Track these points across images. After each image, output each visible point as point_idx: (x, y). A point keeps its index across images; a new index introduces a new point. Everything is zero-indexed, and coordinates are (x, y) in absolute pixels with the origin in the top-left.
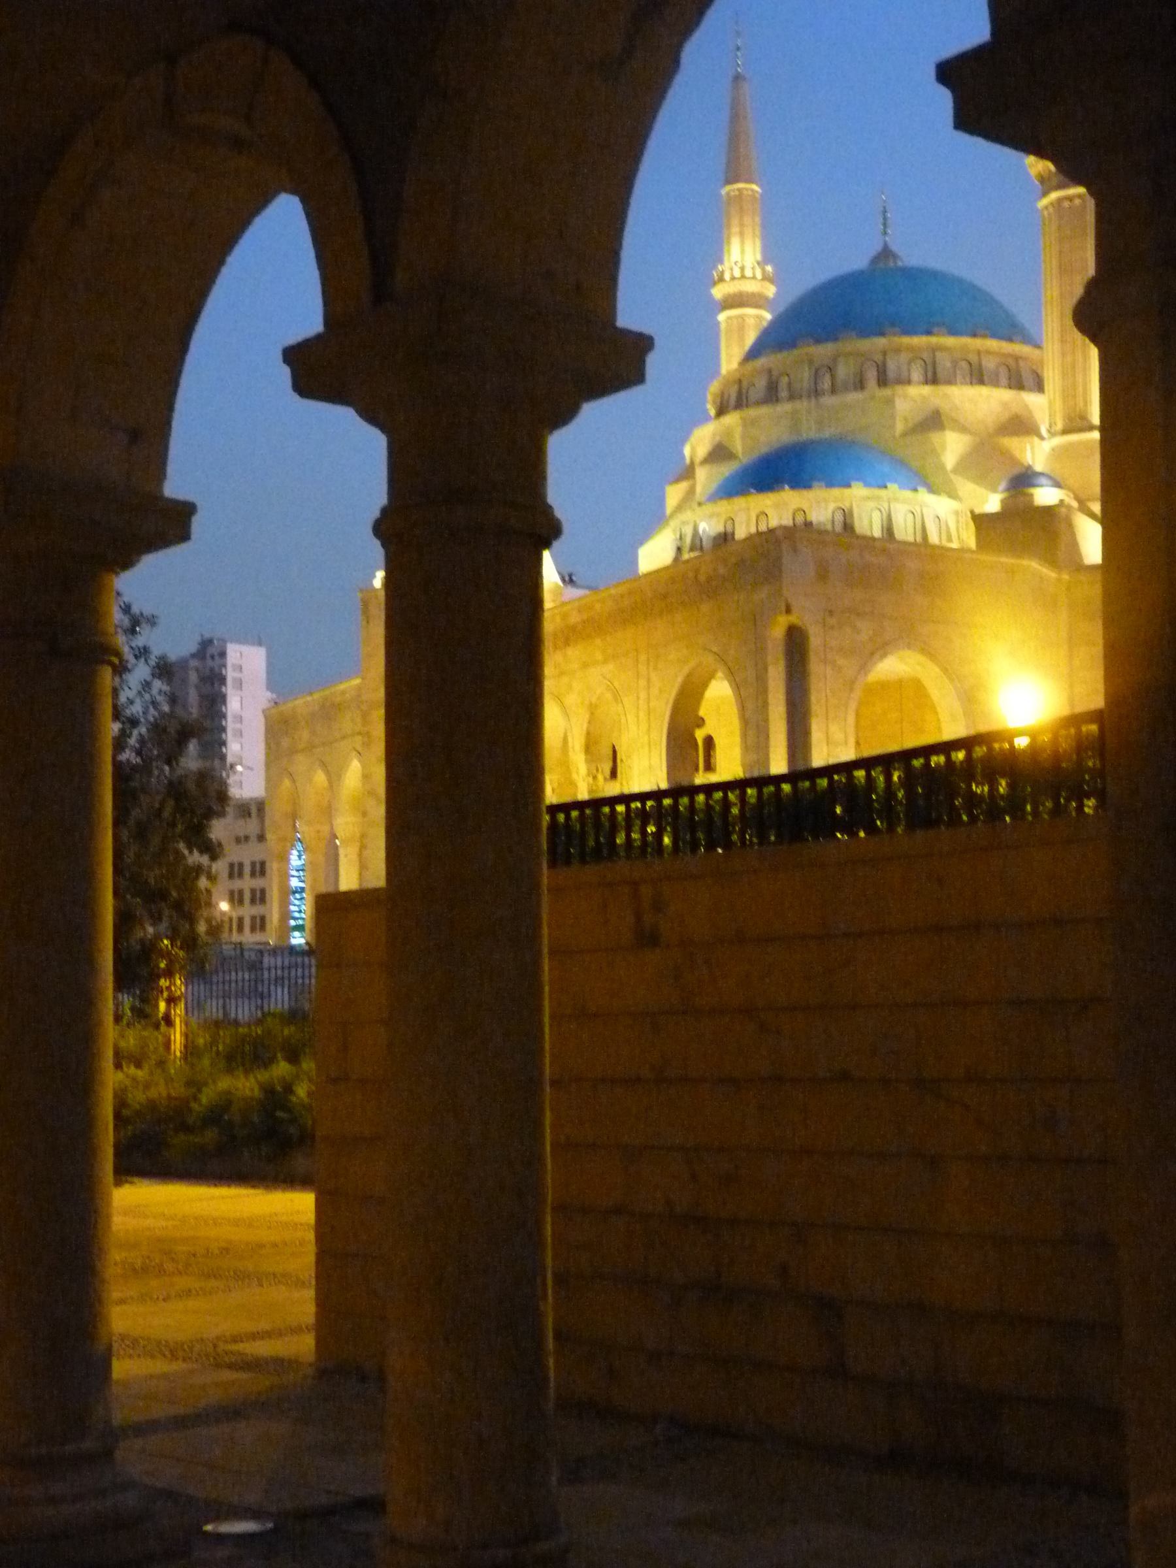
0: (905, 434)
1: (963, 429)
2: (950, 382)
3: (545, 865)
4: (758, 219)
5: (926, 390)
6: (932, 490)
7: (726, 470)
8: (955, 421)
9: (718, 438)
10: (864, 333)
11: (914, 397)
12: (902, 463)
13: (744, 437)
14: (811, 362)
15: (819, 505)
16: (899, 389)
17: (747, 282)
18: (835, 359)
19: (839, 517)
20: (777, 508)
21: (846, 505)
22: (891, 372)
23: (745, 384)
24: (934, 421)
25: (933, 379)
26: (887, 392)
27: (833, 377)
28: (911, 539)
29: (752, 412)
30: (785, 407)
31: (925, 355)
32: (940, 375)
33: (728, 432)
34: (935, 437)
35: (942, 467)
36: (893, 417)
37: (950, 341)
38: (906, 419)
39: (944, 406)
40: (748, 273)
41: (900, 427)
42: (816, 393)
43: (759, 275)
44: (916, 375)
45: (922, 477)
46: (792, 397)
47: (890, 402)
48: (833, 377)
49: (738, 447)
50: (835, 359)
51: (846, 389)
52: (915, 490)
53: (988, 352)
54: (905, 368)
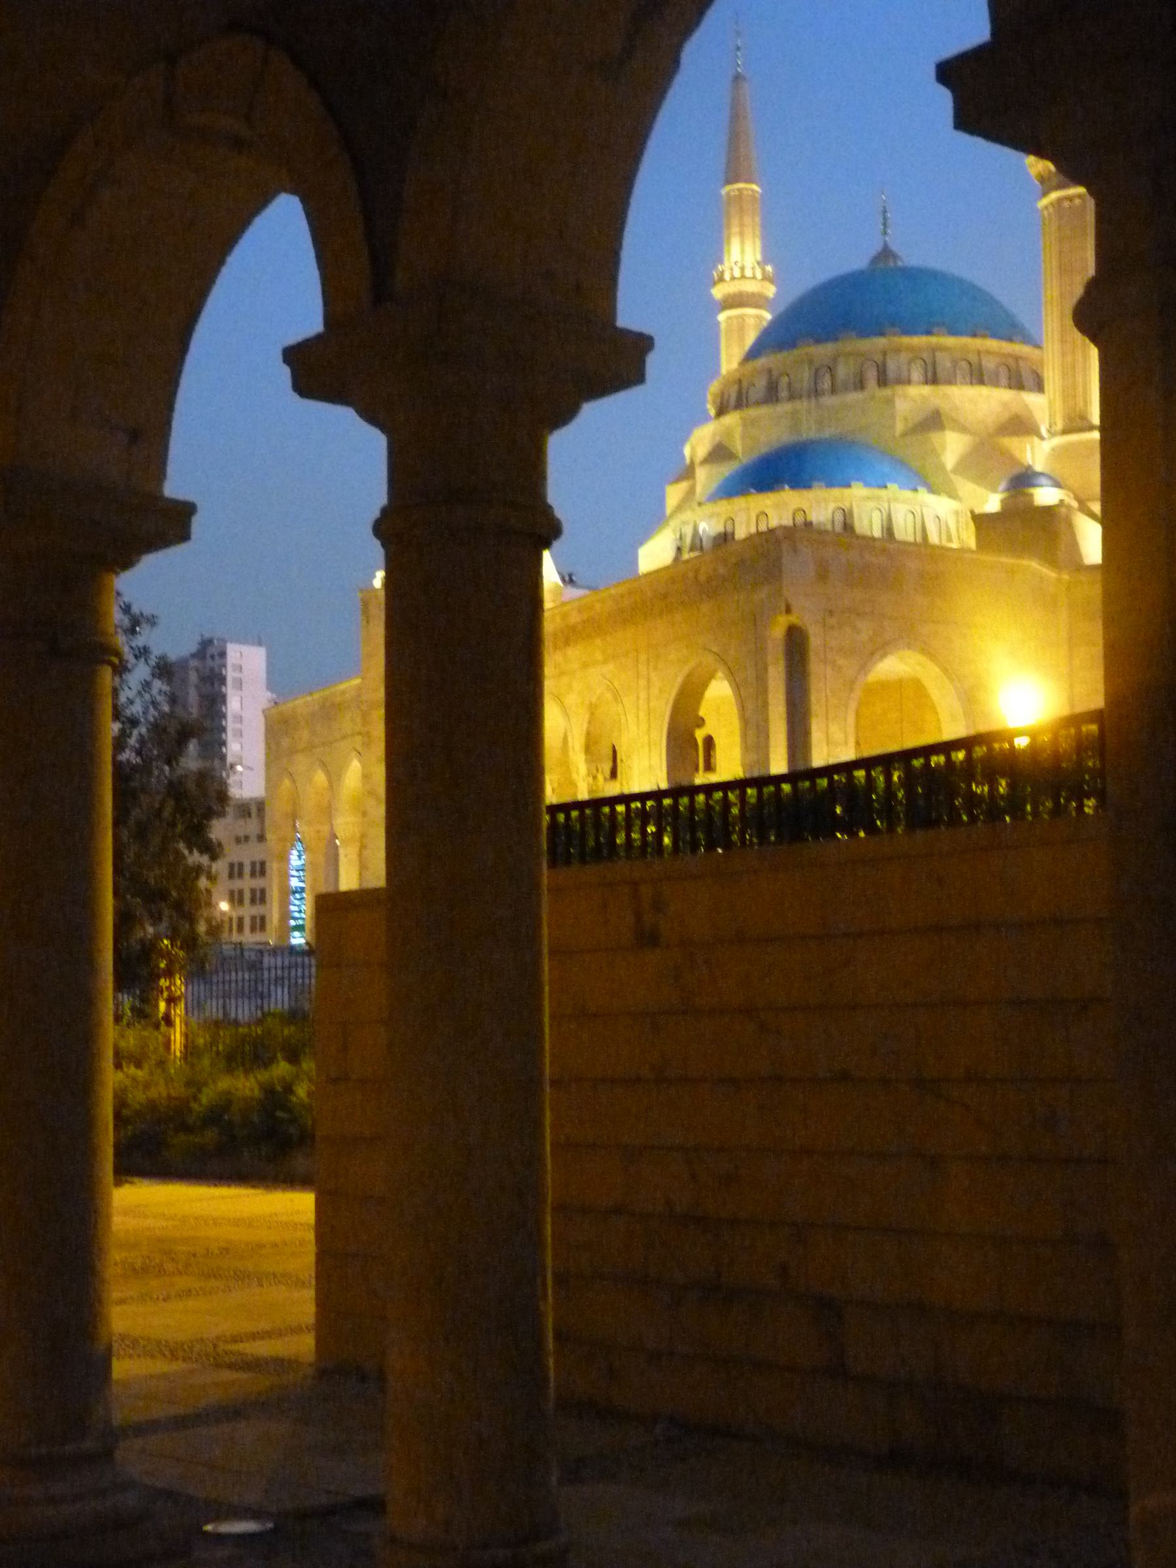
0: (905, 434)
1: (963, 429)
2: (950, 382)
3: (545, 865)
4: (758, 219)
5: (926, 390)
6: (932, 490)
7: (726, 470)
8: (955, 421)
9: (718, 438)
10: (864, 333)
11: (914, 397)
12: (902, 463)
13: (744, 437)
14: (811, 362)
15: (819, 505)
16: (899, 389)
17: (747, 282)
18: (835, 359)
19: (839, 517)
20: (777, 508)
21: (846, 505)
22: (891, 372)
23: (745, 384)
24: (934, 421)
25: (933, 379)
26: (887, 392)
27: (833, 377)
28: (911, 539)
29: (752, 412)
30: (785, 407)
31: (925, 355)
32: (940, 375)
33: (728, 432)
34: (935, 437)
35: (942, 467)
36: (893, 417)
37: (950, 341)
38: (906, 419)
39: (944, 406)
40: (748, 273)
41: (900, 427)
42: (816, 393)
43: (759, 275)
44: (916, 375)
45: (922, 477)
46: (792, 397)
47: (890, 402)
48: (833, 377)
49: (738, 447)
50: (835, 359)
51: (846, 389)
52: (915, 490)
53: (988, 352)
54: (905, 368)
